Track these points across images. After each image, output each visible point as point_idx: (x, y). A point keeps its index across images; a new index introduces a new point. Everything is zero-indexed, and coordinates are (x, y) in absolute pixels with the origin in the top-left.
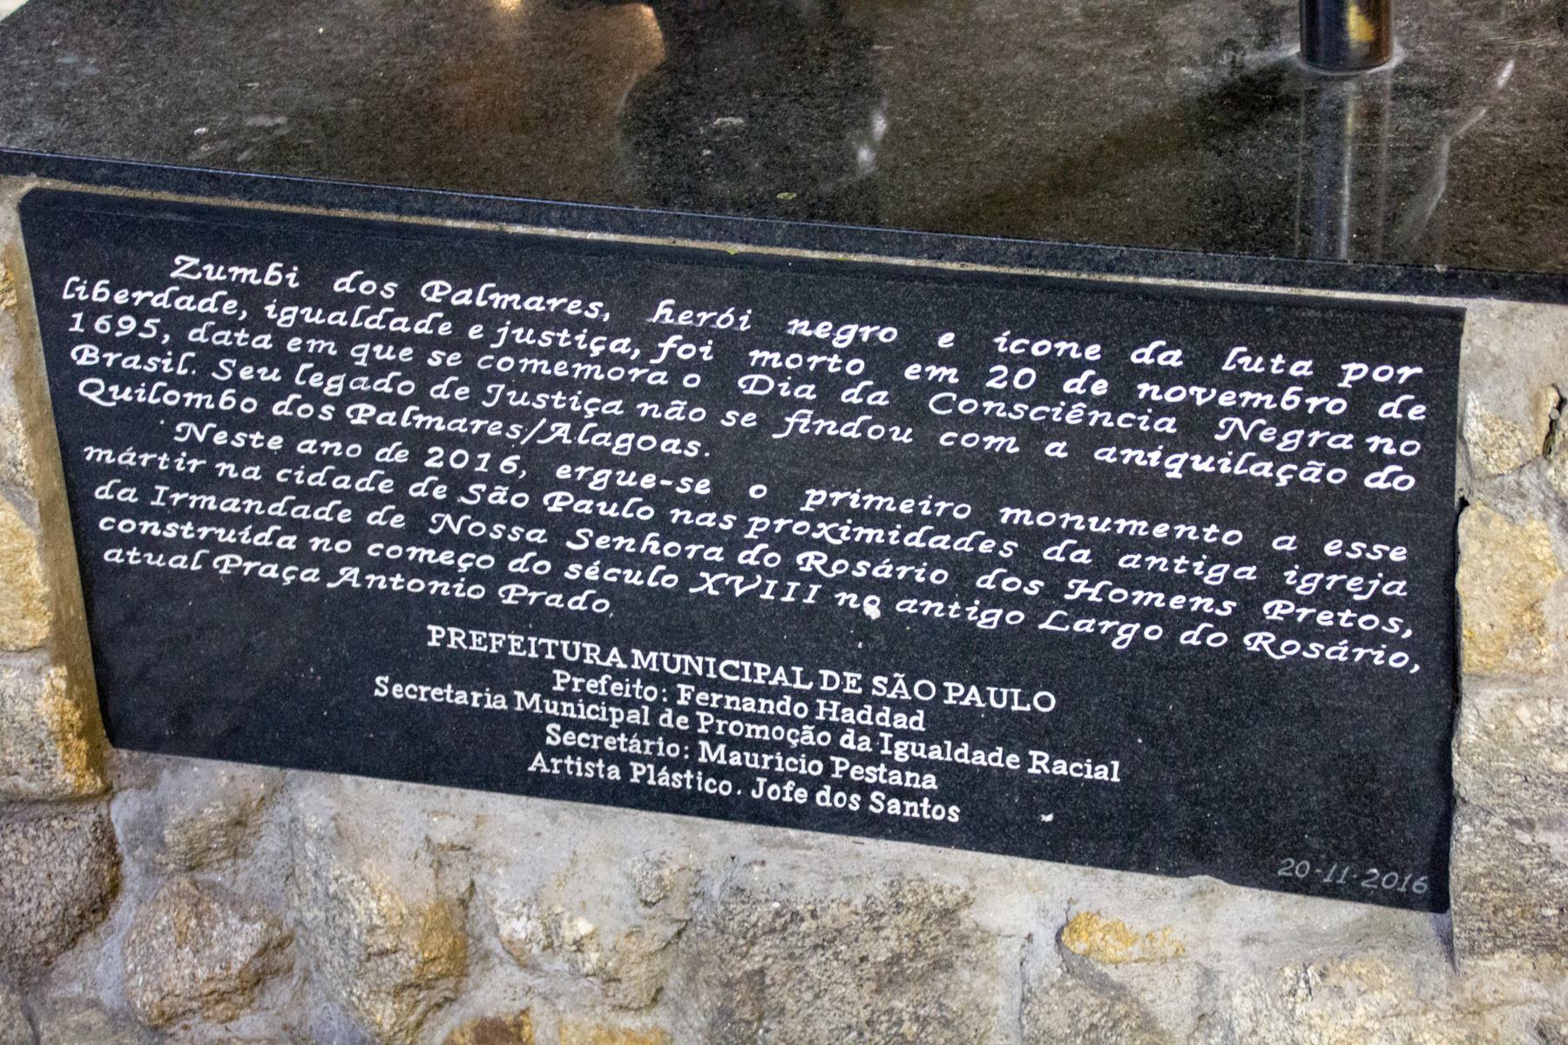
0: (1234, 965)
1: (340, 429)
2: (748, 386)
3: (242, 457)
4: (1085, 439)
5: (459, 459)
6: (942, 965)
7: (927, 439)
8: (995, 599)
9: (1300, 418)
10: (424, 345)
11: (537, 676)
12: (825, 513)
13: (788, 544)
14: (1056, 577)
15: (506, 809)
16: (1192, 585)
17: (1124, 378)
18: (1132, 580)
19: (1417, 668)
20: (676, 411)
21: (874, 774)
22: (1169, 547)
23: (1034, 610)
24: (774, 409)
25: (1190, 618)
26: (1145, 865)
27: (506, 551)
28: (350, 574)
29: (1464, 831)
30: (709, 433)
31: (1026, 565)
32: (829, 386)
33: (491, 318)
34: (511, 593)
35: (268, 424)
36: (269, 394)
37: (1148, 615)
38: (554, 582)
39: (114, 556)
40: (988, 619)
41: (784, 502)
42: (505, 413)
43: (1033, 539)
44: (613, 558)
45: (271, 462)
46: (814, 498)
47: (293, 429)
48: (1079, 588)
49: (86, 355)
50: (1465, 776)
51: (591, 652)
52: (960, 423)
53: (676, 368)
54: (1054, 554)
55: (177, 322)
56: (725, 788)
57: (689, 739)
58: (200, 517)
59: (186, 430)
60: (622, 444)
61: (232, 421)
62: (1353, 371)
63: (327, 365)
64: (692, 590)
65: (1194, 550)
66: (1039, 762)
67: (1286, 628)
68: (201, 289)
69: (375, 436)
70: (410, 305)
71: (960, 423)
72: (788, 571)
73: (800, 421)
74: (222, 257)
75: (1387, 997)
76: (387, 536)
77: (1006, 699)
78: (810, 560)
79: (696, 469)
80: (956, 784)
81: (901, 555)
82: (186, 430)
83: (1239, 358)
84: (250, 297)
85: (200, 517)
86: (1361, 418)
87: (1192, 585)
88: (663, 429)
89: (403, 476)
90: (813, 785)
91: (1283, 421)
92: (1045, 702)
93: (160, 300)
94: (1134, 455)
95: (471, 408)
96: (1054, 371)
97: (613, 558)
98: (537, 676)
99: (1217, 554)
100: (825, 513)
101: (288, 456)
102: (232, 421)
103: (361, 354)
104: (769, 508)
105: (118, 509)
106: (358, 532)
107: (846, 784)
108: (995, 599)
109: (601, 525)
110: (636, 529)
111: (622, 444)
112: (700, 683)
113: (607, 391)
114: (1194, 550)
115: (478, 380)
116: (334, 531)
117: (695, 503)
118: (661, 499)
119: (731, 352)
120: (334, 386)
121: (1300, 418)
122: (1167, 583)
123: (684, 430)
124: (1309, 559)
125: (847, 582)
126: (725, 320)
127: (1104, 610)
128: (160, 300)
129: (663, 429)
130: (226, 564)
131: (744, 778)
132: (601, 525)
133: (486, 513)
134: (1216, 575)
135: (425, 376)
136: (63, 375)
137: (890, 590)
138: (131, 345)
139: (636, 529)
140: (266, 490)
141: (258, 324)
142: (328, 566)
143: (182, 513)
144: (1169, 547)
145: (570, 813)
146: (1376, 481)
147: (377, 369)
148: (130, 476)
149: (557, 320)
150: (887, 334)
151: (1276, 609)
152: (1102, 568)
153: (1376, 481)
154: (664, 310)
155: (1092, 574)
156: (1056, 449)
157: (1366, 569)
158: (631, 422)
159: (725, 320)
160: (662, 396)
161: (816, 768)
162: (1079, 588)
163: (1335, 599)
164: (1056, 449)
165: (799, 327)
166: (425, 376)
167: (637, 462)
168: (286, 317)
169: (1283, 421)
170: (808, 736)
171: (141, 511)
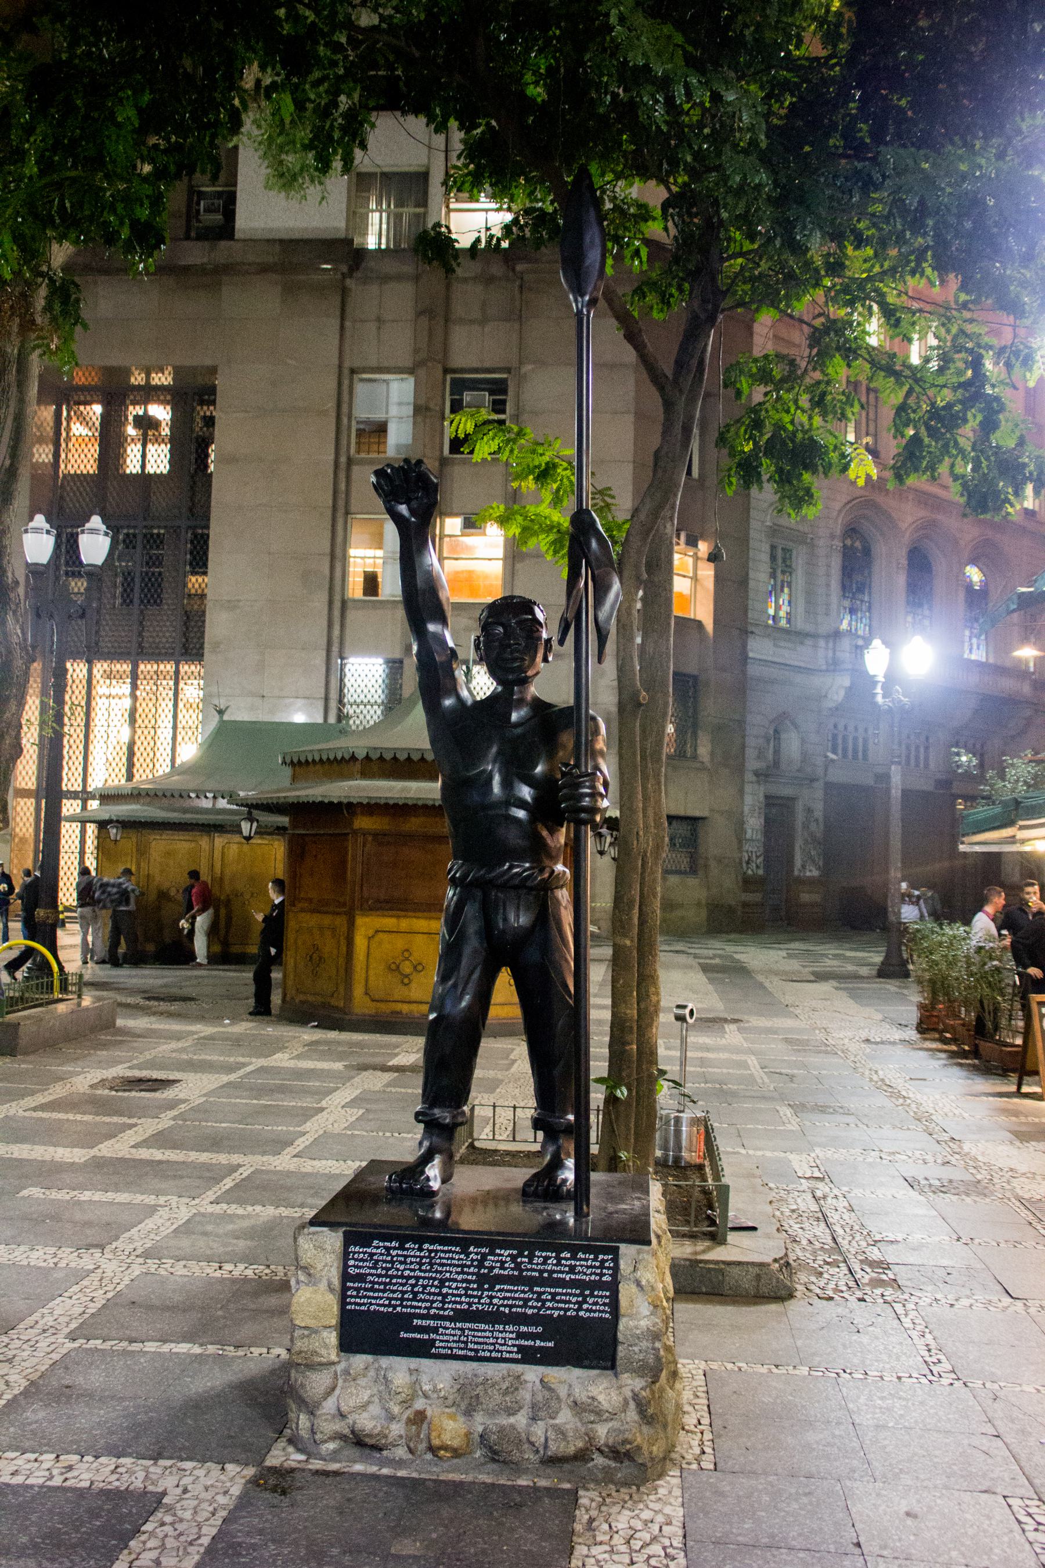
0: (575, 1383)
1: (402, 1277)
2: (487, 1264)
3: (380, 1284)
4: (552, 1272)
5: (426, 1282)
6: (517, 1389)
7: (521, 1271)
8: (532, 1307)
9: (591, 1267)
10: (422, 1258)
11: (435, 1330)
12: (500, 1290)
13: (491, 1297)
14: (544, 1301)
15: (425, 1363)
16: (570, 1302)
17: (559, 1259)
18: (558, 1302)
19: (521, 814)
20: (472, 1270)
21: (504, 1348)
22: (566, 1294)
23: (539, 1309)
24: (492, 1268)
25: (569, 1309)
26: (557, 1365)
27: (433, 1302)
28: (399, 1309)
29: (620, 1348)
30: (477, 1274)
31: (538, 1300)
32: (503, 1263)
33: (436, 1251)
34: (432, 1311)
35: (386, 1276)
36: (387, 1269)
37: (561, 1309)
38: (443, 1309)
39: (349, 1307)
40: (530, 1312)
41: (491, 1288)
42: (437, 1272)
43: (540, 1294)
44: (455, 1302)
45: (385, 1284)
46: (498, 1287)
47: (392, 1277)
48: (548, 1304)
49: (351, 1263)
50: (620, 1337)
51: (448, 1324)
52: (528, 1270)
53: (472, 1260)
54: (544, 1297)
55: (372, 1255)
56: (473, 1354)
57: (466, 1343)
58: (369, 1297)
59: (370, 1278)
60: (460, 1277)
61: (379, 1276)
62: (601, 1257)
63: (401, 1263)
64: (403, 1335)
65: (570, 1295)
66: (538, 1343)
67: (587, 1310)
68: (378, 1248)
69: (409, 1278)
70: (420, 1249)
71: (528, 1270)
72: (491, 1303)
73: (496, 1271)
74: (384, 1241)
75: (605, 1385)
76: (408, 1300)
77: (532, 1329)
78: (495, 1301)
79: (474, 1282)
80: (521, 1349)
81: (514, 1299)
82: (370, 1278)
83: (581, 1255)
84: (388, 1249)
85: (369, 1297)
86: (602, 1267)
87: (570, 1302)
88: (468, 1274)
89: (413, 1286)
90: (491, 1351)
91: (588, 1267)
92: (540, 1329)
93: (369, 1250)
94: (560, 1275)
95: (430, 1271)
96: (546, 1258)
97: (455, 1302)
98: (435, 1330)
99: (575, 1295)
100: (500, 1290)
101: (390, 1283)
102: (379, 1276)
103: (408, 1260)
104: (488, 1290)
105: (352, 1296)
106: (402, 1299)
107: (498, 1351)
108: (532, 1307)
109: (453, 1295)
110: (460, 1296)
111: (460, 1277)
112: (470, 1329)
113: (458, 1266)
114: (570, 1295)
115: (431, 1264)
116: (396, 1299)
117: (473, 1289)
118: (466, 1289)
119: (484, 1257)
120: (402, 1267)
121: (591, 1267)
122: (566, 1302)
123: (473, 1274)
124: (592, 1295)
125: (502, 1305)
126: (483, 1250)
127: (553, 1309)
128: (369, 1250)
129: (468, 1274)
130: (372, 1308)
131: (476, 1351)
132: (453, 1295)
133: (430, 1294)
134: (574, 1300)
135: (421, 1264)
136: (346, 1266)
137: (511, 1306)
138: (362, 1260)
139: (460, 1296)
140: (384, 1291)
141: (389, 1254)
142: (395, 1307)
143: (365, 1297)
144: (566, 1294)
145: (439, 1362)
146: (604, 1279)
147: (411, 1263)
148: (355, 1289)
149: (450, 1251)
150: (515, 1252)
151: (585, 1306)
152: (553, 1299)
153: (604, 1279)
154: (471, 1249)
155: (550, 1301)
156: (546, 1275)
157: (602, 1297)
158: (463, 1272)
159: (483, 1250)
160: (469, 1267)
161: (491, 1348)
162: (548, 1304)
163: (596, 1303)
164: (546, 1275)
165: (498, 1251)
166: (421, 1264)
167: (463, 1281)
168: (394, 1253)
169: (588, 1267)
170: (491, 1340)
171: (357, 1297)
